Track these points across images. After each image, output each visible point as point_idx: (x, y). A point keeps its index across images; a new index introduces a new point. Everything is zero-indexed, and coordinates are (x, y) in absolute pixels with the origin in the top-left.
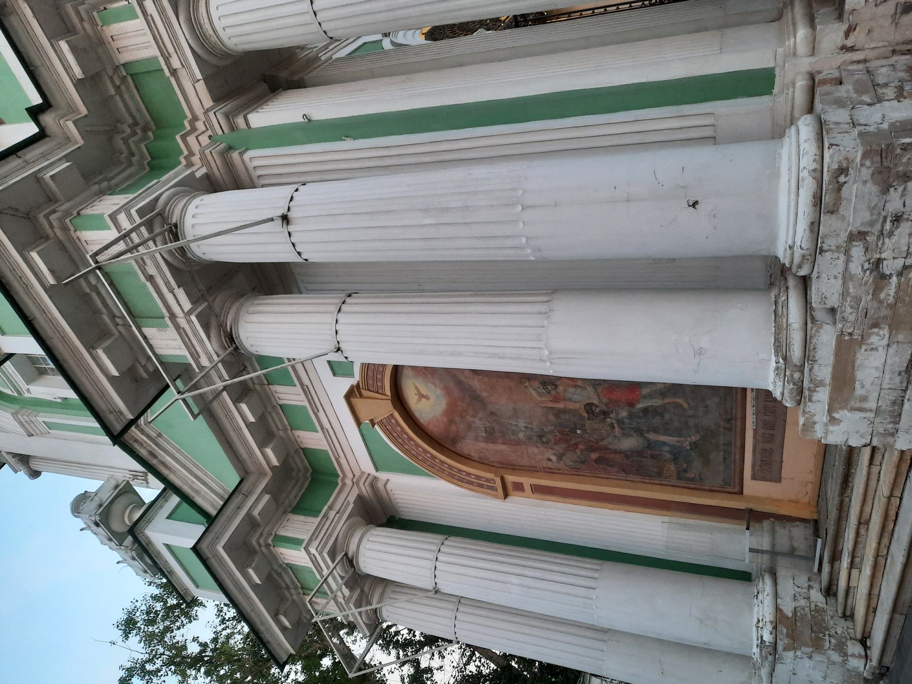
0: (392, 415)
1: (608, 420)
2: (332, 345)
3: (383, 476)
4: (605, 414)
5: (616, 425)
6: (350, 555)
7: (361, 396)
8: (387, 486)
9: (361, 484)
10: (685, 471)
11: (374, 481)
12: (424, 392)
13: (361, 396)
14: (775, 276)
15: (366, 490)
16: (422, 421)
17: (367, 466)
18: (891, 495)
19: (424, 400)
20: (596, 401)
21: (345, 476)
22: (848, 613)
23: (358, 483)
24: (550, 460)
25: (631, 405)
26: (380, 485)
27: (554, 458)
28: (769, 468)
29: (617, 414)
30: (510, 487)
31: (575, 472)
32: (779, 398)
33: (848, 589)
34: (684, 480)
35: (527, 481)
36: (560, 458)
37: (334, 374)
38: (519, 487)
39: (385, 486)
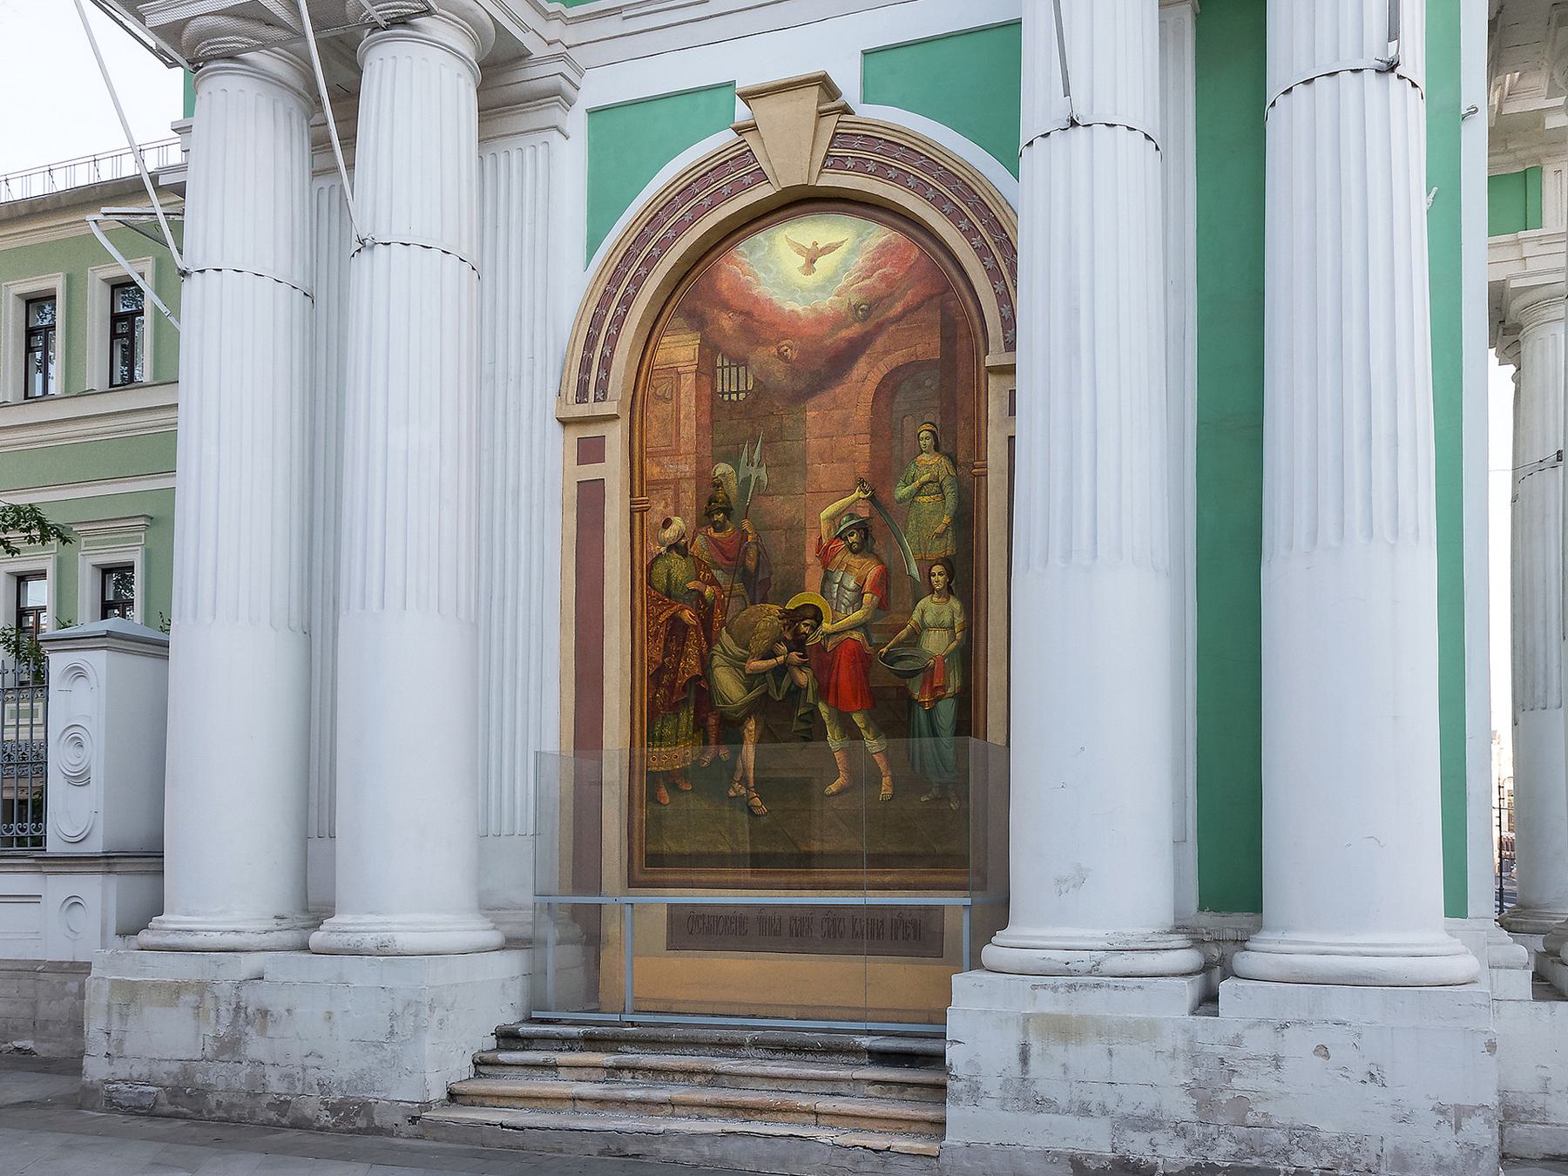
0: (761, 176)
1: (784, 648)
2: (1082, 114)
3: (576, 121)
4: (798, 643)
5: (772, 662)
6: (421, 21)
7: (822, 114)
8: (556, 133)
9: (561, 67)
10: (674, 787)
11: (557, 96)
12: (821, 263)
13: (822, 114)
14: (312, 906)
15: (538, 75)
16: (742, 247)
17: (605, 84)
18: (817, 1114)
19: (802, 261)
20: (826, 626)
21: (570, 21)
22: (482, 1069)
23: (558, 57)
24: (667, 523)
25: (823, 692)
26: (555, 115)
27: (669, 534)
28: (692, 931)
29: (800, 666)
30: (592, 432)
31: (645, 574)
32: (989, 953)
33: (555, 1067)
34: (651, 785)
35: (613, 470)
36: (676, 547)
37: (865, 53)
38: (590, 451)
39: (556, 127)
